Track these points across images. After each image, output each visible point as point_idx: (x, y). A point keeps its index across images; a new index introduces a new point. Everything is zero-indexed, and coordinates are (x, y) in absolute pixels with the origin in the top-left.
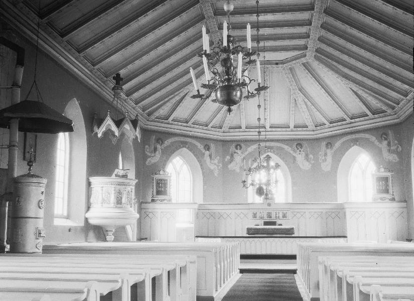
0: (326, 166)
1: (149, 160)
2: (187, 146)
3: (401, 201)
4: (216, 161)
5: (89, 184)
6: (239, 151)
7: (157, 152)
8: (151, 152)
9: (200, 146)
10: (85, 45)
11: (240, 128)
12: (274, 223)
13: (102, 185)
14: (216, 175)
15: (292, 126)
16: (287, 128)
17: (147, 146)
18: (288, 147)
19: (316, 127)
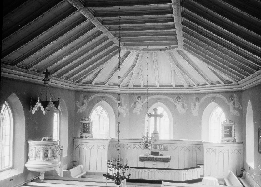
0: (195, 113)
1: (79, 110)
2: (105, 99)
3: (238, 143)
4: (125, 107)
5: (27, 144)
6: (139, 101)
7: (85, 105)
8: (81, 105)
9: (114, 98)
10: (23, 56)
11: (140, 86)
12: (157, 154)
13: (35, 146)
14: (124, 116)
15: (174, 85)
16: (170, 86)
17: (77, 102)
18: (171, 99)
19: (189, 86)
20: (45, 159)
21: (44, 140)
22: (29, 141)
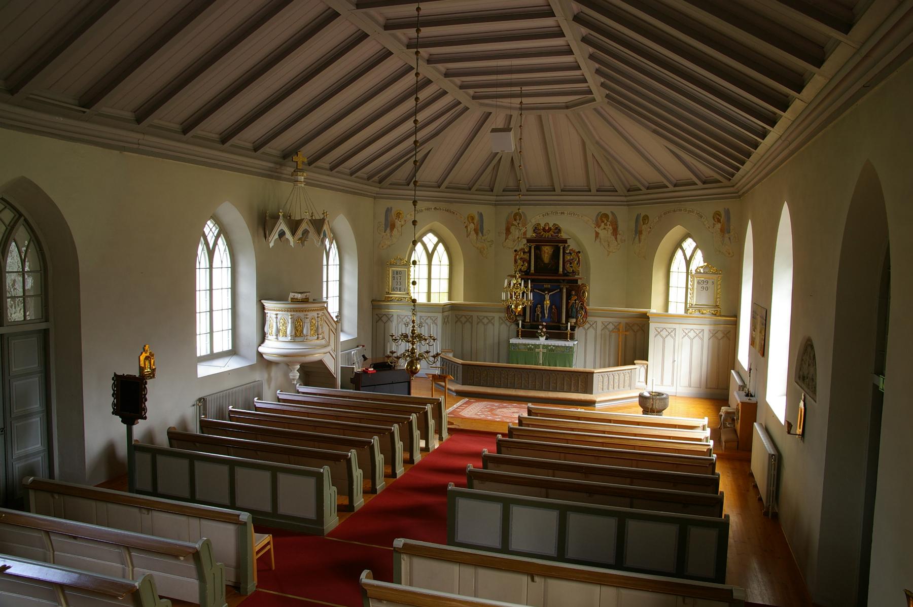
5: (263, 308)
20: (298, 339)
21: (294, 301)
22: (268, 304)
